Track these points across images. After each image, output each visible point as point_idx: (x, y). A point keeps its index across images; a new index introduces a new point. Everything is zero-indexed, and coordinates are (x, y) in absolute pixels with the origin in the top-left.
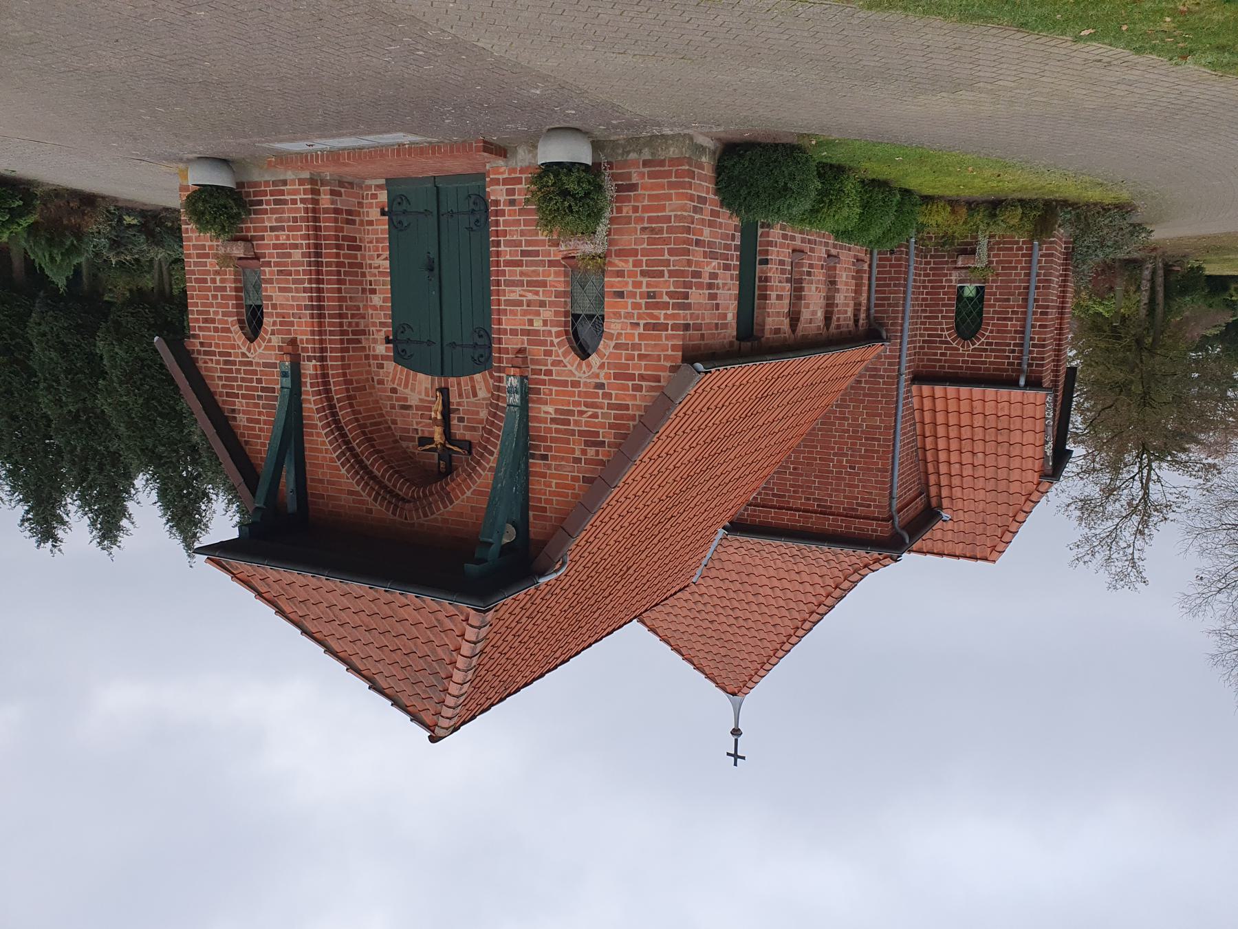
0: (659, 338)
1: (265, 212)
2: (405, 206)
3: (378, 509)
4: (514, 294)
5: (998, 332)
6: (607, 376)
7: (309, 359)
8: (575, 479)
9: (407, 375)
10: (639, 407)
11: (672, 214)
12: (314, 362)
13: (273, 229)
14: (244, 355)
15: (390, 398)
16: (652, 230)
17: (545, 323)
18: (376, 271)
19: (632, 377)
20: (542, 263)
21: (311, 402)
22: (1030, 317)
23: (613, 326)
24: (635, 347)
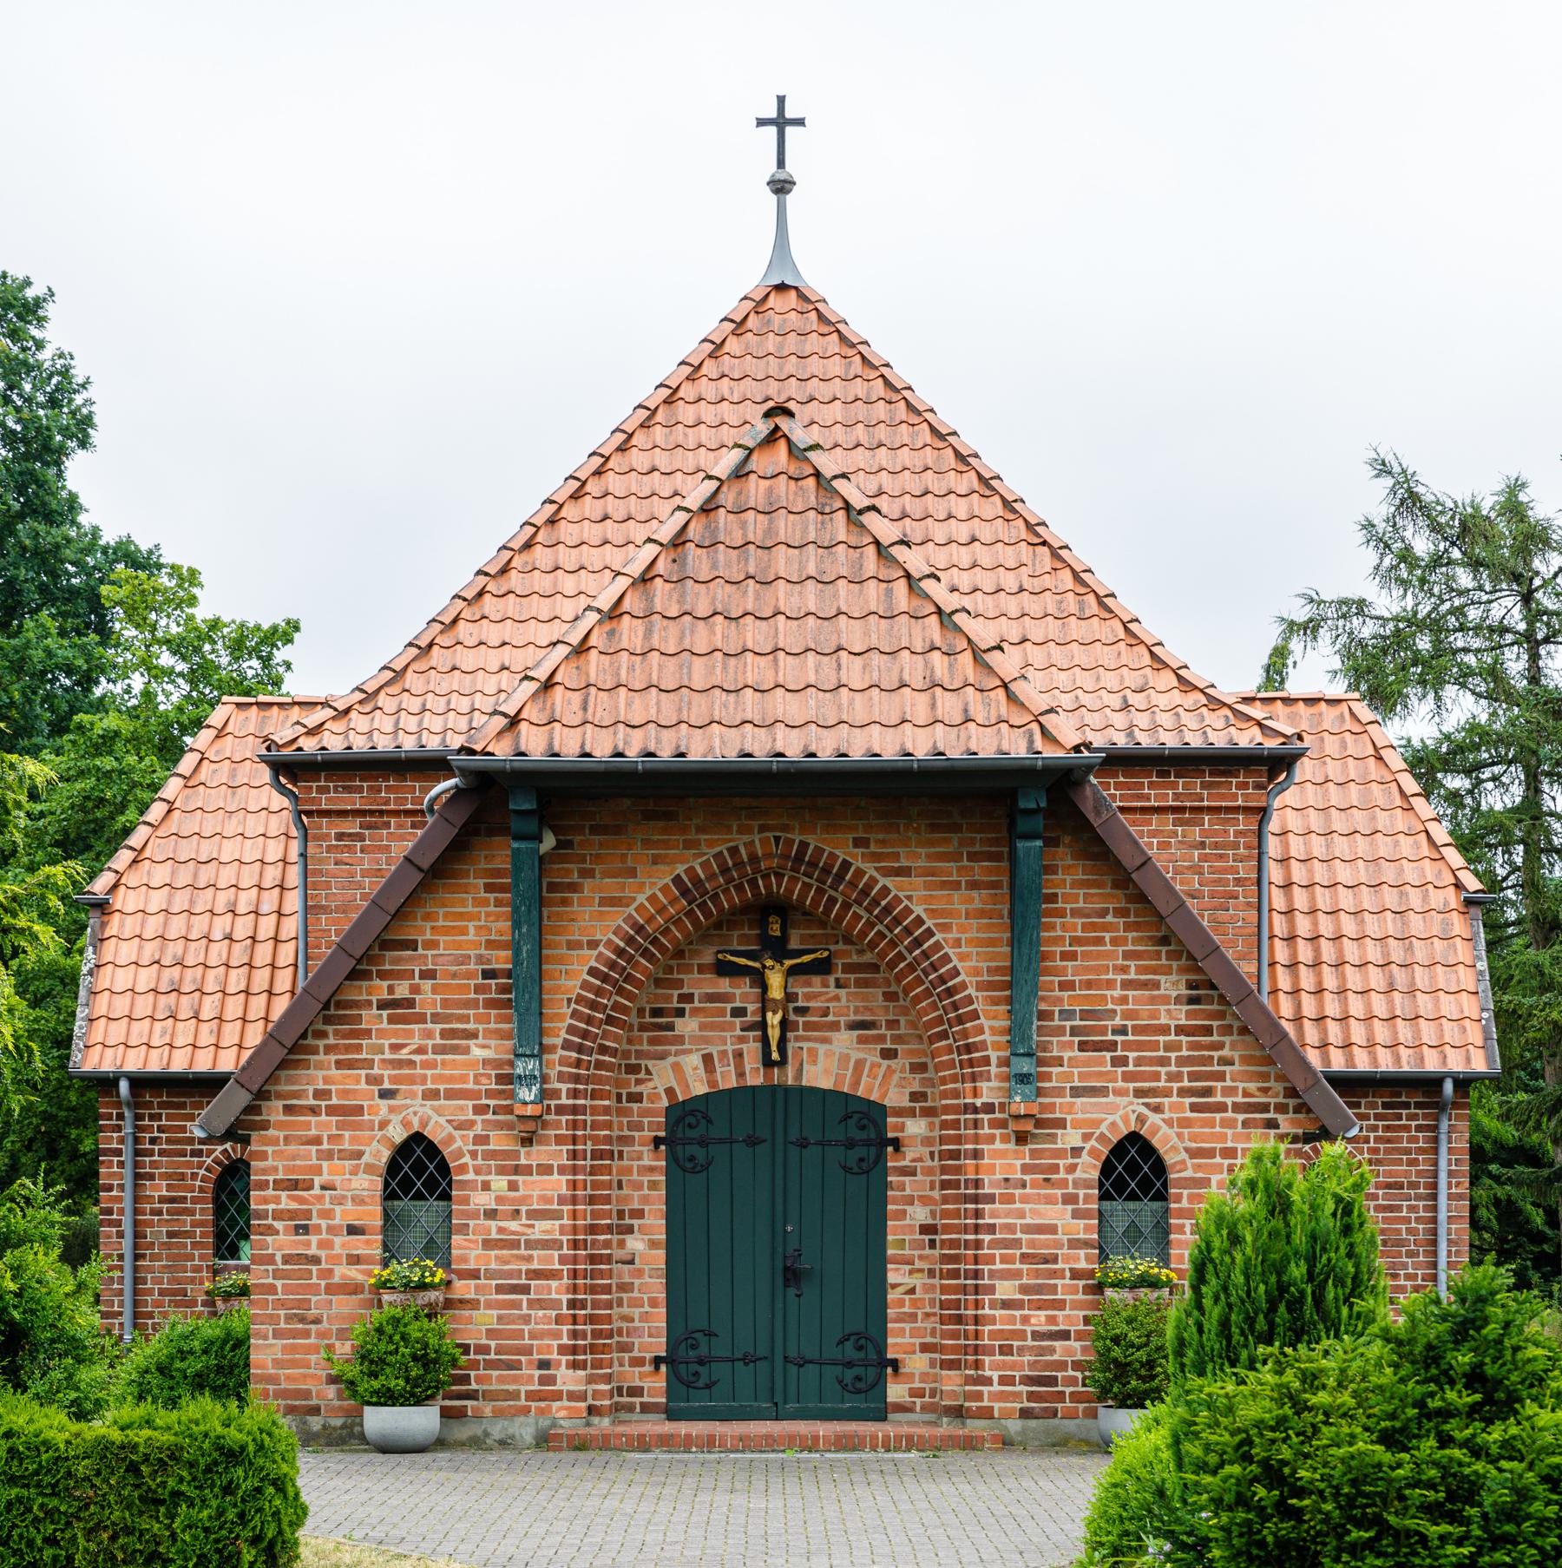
0: (287, 1170)
1: (1077, 1365)
4: (543, 1229)
5: (182, 1177)
6: (373, 1110)
7: (989, 1108)
8: (431, 945)
9: (856, 1083)
10: (320, 1066)
11: (271, 1341)
12: (978, 1102)
13: (1065, 1335)
14: (1157, 1109)
15: (898, 1039)
16: (302, 1320)
17: (486, 1186)
18: (918, 1264)
19: (331, 1110)
20: (490, 1275)
21: (990, 1028)
22: (127, 1204)
23: (369, 1185)
24: (329, 1155)
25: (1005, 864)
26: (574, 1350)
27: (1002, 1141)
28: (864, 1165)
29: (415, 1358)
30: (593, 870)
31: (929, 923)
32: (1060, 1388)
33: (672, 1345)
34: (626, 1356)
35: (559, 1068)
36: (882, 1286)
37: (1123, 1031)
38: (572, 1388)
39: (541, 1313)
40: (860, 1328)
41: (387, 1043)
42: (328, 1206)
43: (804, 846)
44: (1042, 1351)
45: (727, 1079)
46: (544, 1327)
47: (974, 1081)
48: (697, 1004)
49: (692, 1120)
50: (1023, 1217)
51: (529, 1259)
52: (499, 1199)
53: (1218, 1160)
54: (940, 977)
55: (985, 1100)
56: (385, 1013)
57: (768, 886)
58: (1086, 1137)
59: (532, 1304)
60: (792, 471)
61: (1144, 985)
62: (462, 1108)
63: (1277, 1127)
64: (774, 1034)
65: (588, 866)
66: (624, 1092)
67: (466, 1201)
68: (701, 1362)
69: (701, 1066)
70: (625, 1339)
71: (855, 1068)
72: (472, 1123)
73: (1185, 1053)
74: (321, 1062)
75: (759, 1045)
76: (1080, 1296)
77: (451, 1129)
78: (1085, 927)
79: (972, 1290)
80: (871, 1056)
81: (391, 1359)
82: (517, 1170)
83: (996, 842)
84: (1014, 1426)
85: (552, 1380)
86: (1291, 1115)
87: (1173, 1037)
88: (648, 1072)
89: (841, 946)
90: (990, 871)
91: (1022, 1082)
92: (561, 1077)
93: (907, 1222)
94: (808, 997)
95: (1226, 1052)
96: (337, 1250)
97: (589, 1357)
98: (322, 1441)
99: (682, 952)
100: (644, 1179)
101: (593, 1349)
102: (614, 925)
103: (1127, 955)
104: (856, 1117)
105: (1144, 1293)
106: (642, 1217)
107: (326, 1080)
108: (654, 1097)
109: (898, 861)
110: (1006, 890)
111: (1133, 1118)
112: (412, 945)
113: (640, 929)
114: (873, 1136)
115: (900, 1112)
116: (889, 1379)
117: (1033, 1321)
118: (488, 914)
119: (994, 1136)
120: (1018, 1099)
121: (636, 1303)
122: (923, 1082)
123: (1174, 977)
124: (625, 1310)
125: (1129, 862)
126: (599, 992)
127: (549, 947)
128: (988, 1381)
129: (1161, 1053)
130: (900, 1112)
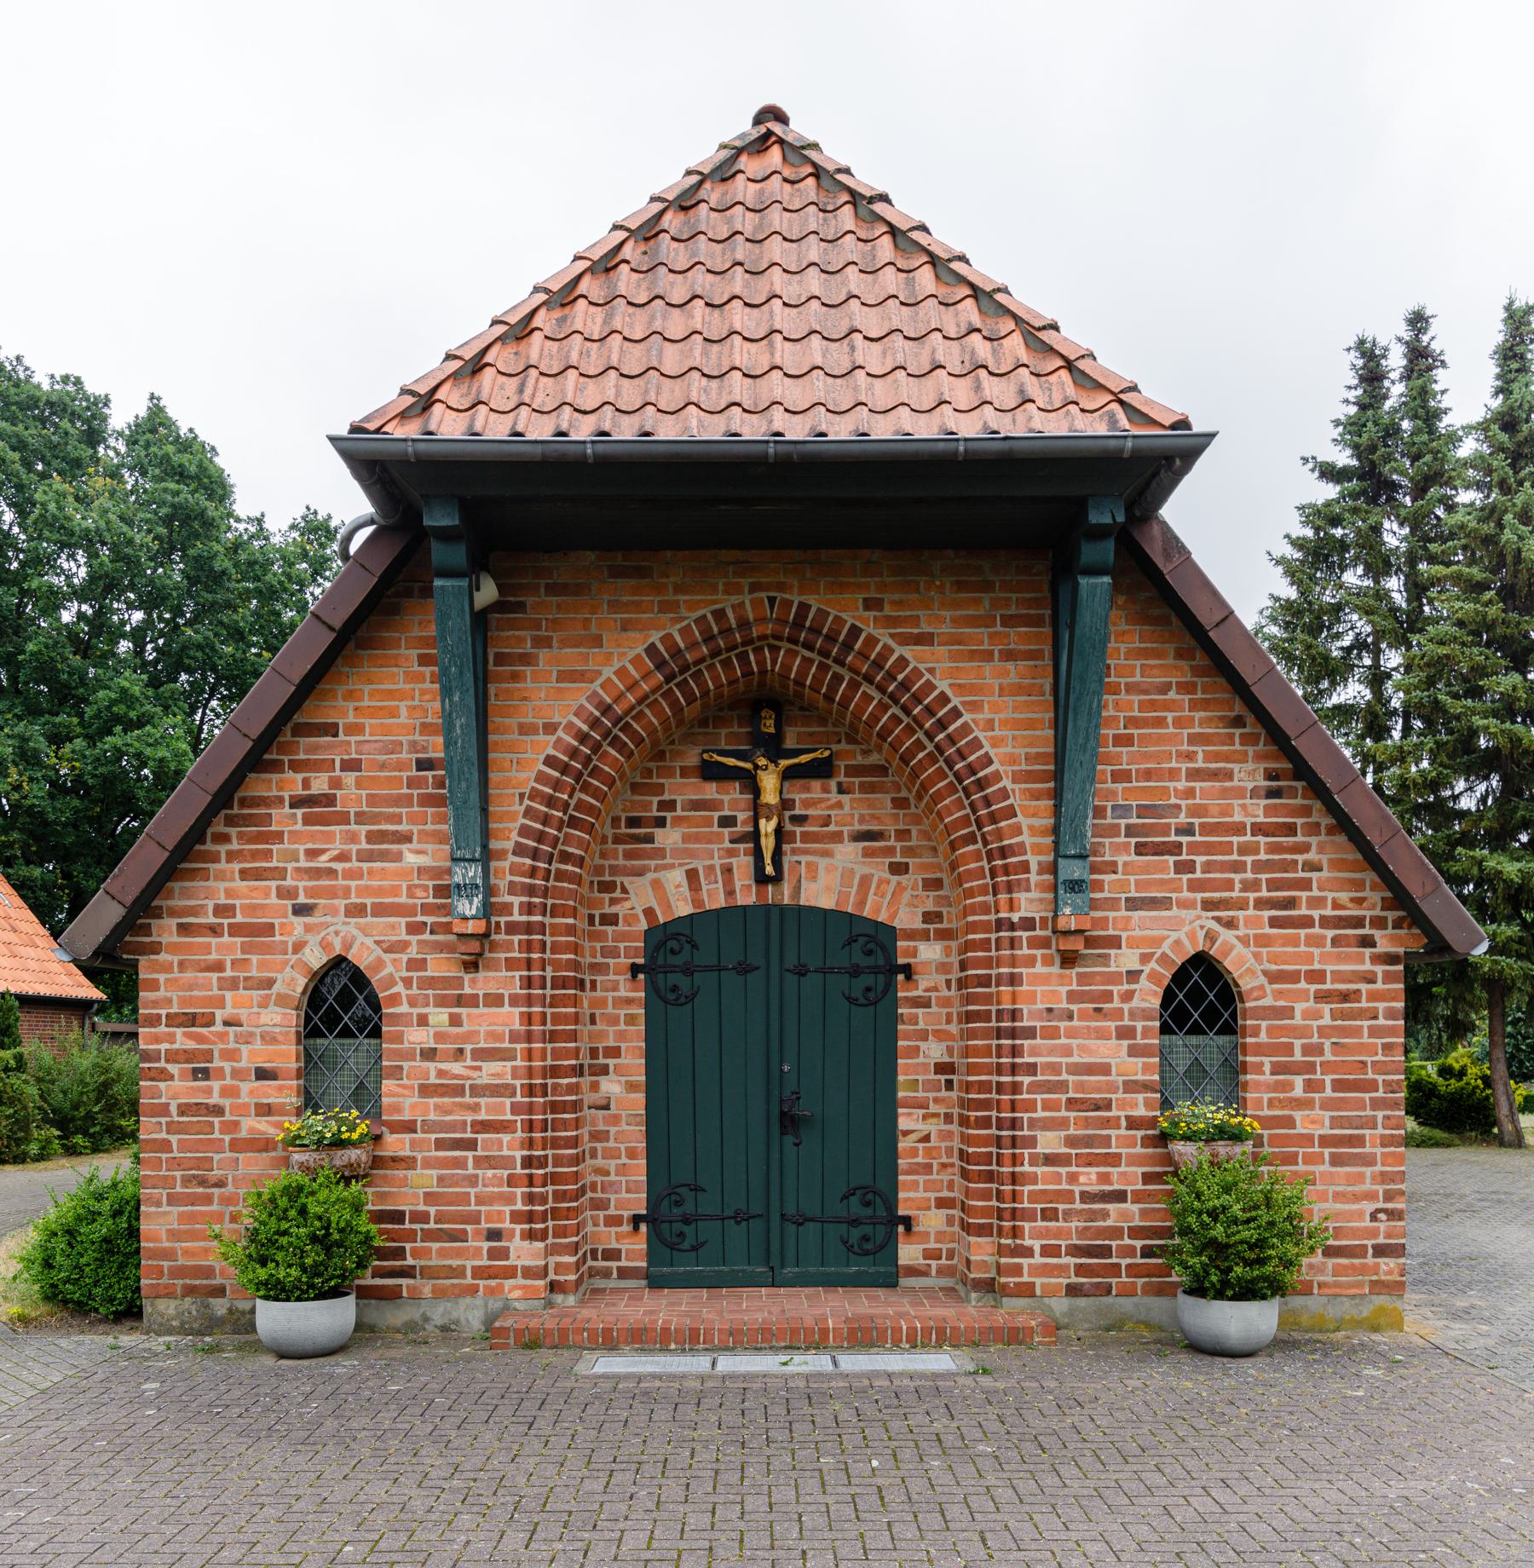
0: (183, 1002)
1: (1135, 1233)
2: (855, 1234)
4: (491, 1072)
6: (286, 929)
7: (1028, 924)
8: (355, 729)
10: (221, 876)
11: (165, 1208)
12: (1015, 917)
13: (1120, 1196)
14: (1230, 924)
15: (909, 852)
16: (203, 1182)
17: (423, 1021)
18: (933, 1108)
19: (235, 930)
20: (429, 1127)
21: (1029, 827)
24: (233, 984)
25: (1047, 630)
26: (530, 1217)
28: (872, 995)
29: (314, 1239)
30: (551, 638)
31: (955, 701)
32: (1114, 1260)
33: (653, 1202)
34: (601, 1214)
35: (509, 878)
36: (892, 1134)
37: (1188, 830)
38: (527, 1263)
39: (490, 1173)
41: (302, 848)
42: (232, 1045)
43: (804, 607)
44: (1093, 1216)
45: (715, 899)
46: (493, 1190)
47: (1010, 891)
48: (679, 812)
49: (673, 944)
50: (1070, 1054)
51: (475, 1108)
52: (439, 1037)
53: (1303, 985)
54: (969, 766)
55: (1023, 914)
56: (299, 812)
57: (761, 663)
58: (1145, 958)
59: (478, 1162)
60: (787, 173)
61: (1214, 775)
62: (393, 927)
63: (1374, 945)
64: (768, 844)
66: (597, 913)
67: (399, 1038)
68: (686, 1221)
69: (685, 883)
70: (599, 1195)
71: (861, 884)
72: (406, 944)
73: (1263, 856)
74: (223, 871)
75: (751, 859)
76: (1139, 1150)
77: (380, 952)
78: (1143, 706)
80: (879, 870)
81: (284, 1240)
82: (460, 1001)
83: (1037, 603)
84: (1060, 1305)
85: (503, 1254)
86: (1390, 931)
87: (1249, 838)
88: (624, 890)
89: (843, 746)
91: (1073, 889)
92: (513, 889)
93: (921, 1060)
94: (807, 804)
95: (1312, 856)
96: (245, 1098)
97: (550, 1223)
98: (228, 1328)
100: (620, 1012)
101: (556, 1214)
102: (575, 705)
103: (1193, 739)
104: (862, 940)
105: (1222, 1148)
106: (619, 1056)
107: (229, 893)
108: (631, 919)
109: (918, 626)
110: (1048, 661)
111: (1201, 934)
112: (332, 730)
113: (606, 710)
115: (911, 935)
117: (1082, 1179)
118: (423, 692)
120: (1067, 911)
121: (612, 1154)
123: (1250, 766)
124: (599, 1162)
125: (1206, 618)
127: (497, 731)
128: (1029, 1252)
129: (1235, 857)
130: (911, 935)
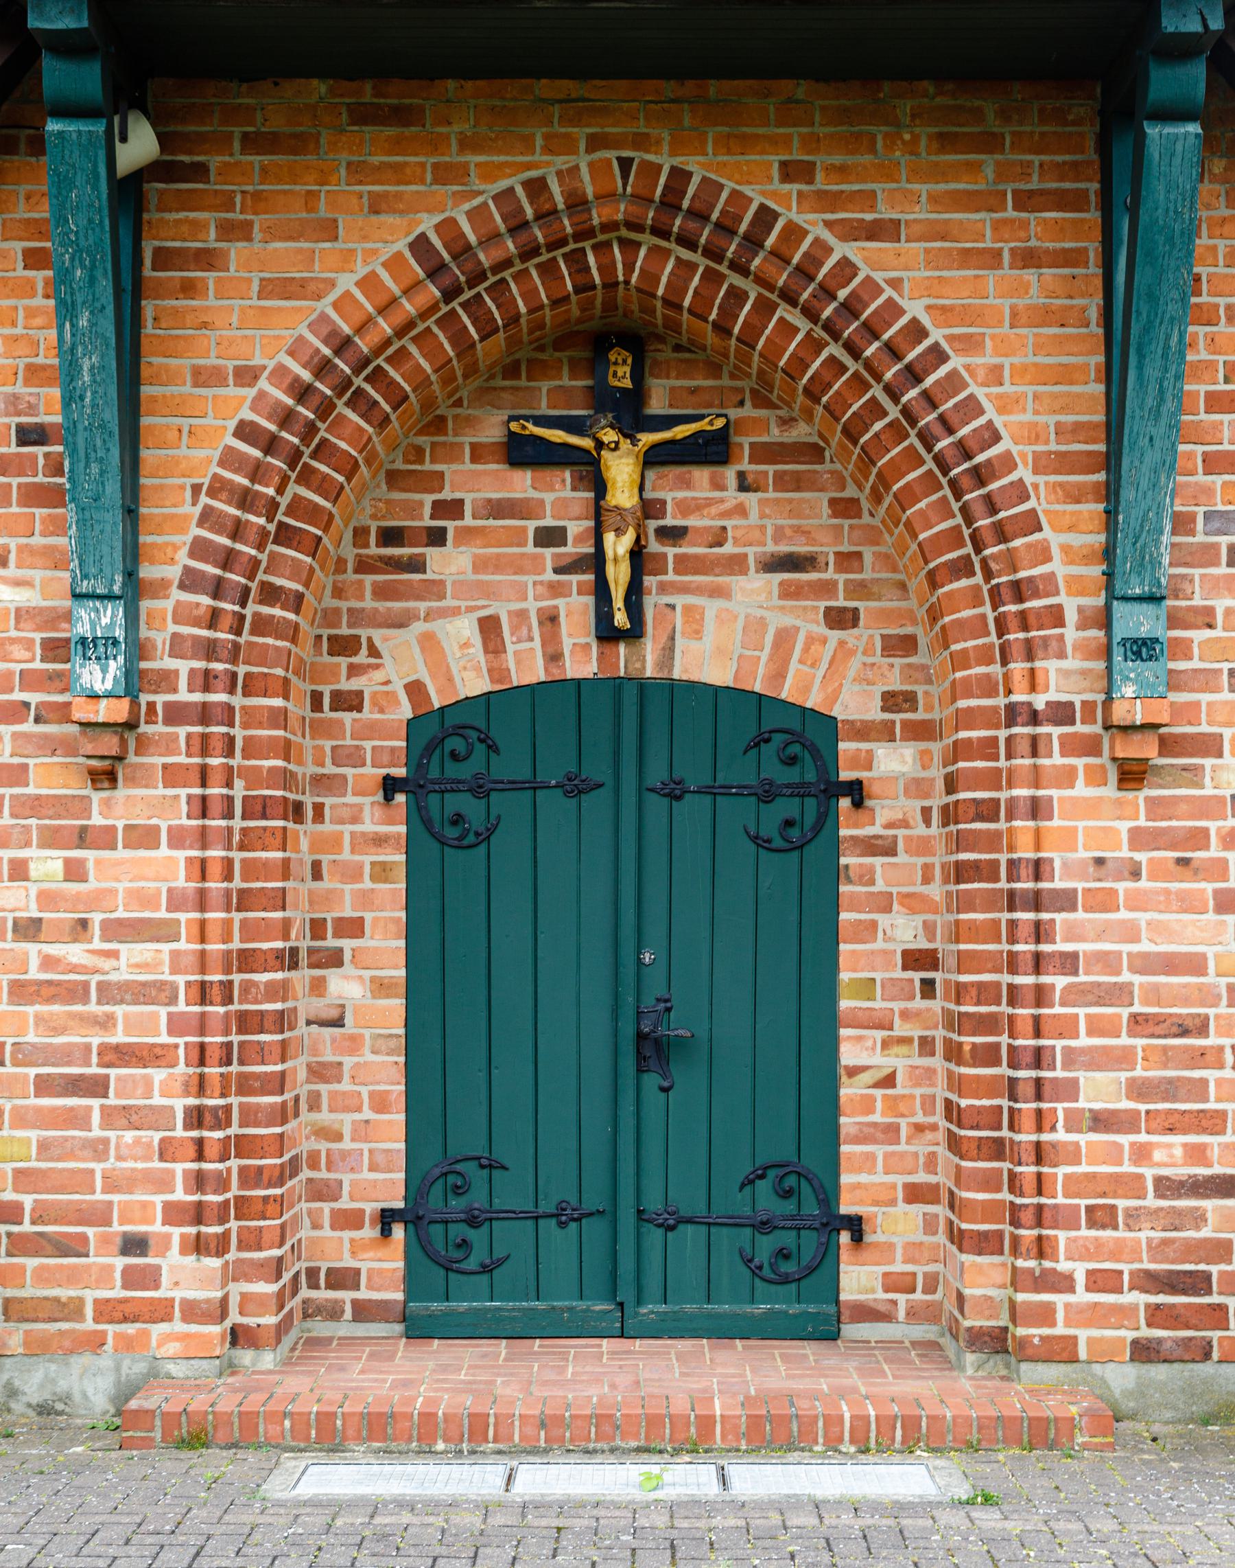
3: (748, 179)
4: (134, 960)
7: (1062, 713)
9: (779, 675)
12: (1040, 702)
15: (860, 590)
21: (1062, 549)
25: (1093, 216)
26: (198, 1214)
27: (1089, 782)
28: (794, 833)
30: (250, 224)
31: (936, 335)
32: (1215, 1299)
33: (417, 1187)
34: (326, 1207)
35: (172, 628)
36: (829, 1073)
38: (192, 1295)
39: (129, 1136)
40: (787, 1153)
43: (680, 176)
44: (1177, 1220)
45: (527, 665)
48: (468, 521)
50: (1136, 939)
52: (47, 899)
55: (1053, 696)
57: (607, 269)
64: (618, 575)
65: (237, 216)
66: (326, 690)
70: (323, 1174)
75: (590, 600)
79: (1030, 1090)
80: (807, 621)
82: (83, 838)
83: (1075, 170)
84: (1122, 1377)
85: (150, 1278)
88: (374, 652)
89: (748, 411)
90: (1059, 230)
91: (1138, 654)
92: (177, 647)
93: (880, 944)
99: (442, 419)
100: (362, 861)
102: (289, 336)
104: (778, 739)
108: (385, 701)
109: (873, 208)
113: (343, 345)
114: (811, 776)
115: (863, 731)
116: (844, 1255)
117: (1158, 1156)
119: (1072, 770)
120: (1129, 691)
121: (349, 1104)
122: (909, 672)
124: (325, 1117)
126: (257, 472)
128: (1065, 1283)
130: (863, 731)
